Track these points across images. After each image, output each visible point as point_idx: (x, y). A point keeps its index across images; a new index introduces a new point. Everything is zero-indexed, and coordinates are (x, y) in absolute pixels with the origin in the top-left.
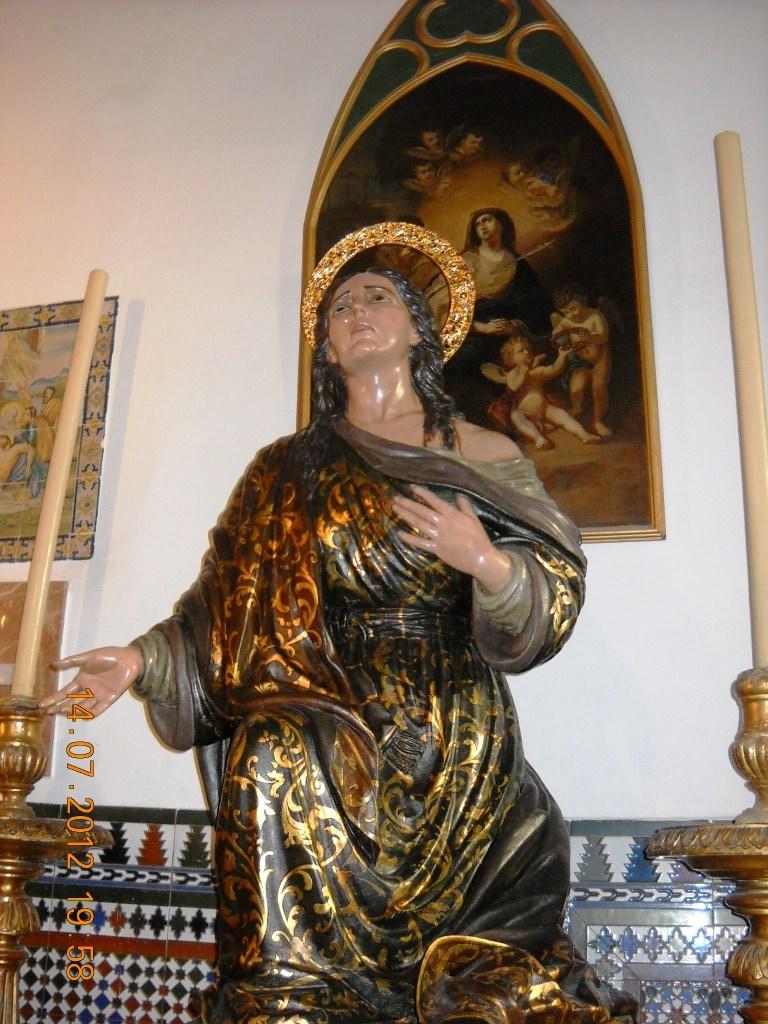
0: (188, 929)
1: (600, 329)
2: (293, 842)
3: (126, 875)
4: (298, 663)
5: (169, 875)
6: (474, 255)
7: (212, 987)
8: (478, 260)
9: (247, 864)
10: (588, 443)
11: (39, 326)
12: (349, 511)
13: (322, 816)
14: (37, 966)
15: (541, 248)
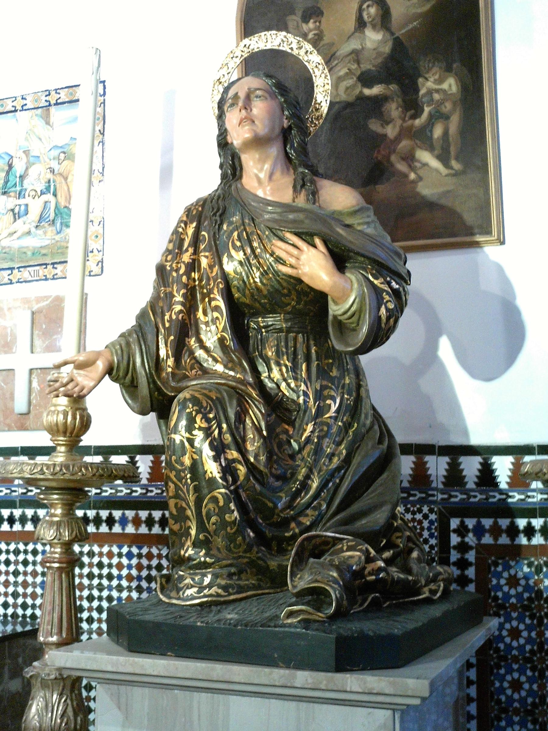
0: (29, 523)
1: (454, 89)
2: (210, 475)
3: (140, 491)
4: (216, 355)
5: (535, 494)
6: (362, 35)
7: (76, 554)
8: (364, 39)
9: (182, 491)
10: (446, 176)
11: (50, 105)
12: (244, 251)
13: (230, 457)
14: (96, 596)
15: (411, 26)
